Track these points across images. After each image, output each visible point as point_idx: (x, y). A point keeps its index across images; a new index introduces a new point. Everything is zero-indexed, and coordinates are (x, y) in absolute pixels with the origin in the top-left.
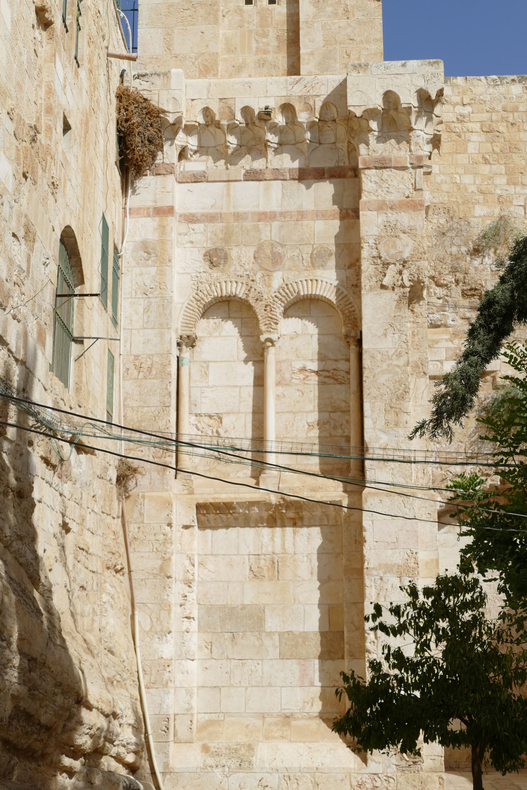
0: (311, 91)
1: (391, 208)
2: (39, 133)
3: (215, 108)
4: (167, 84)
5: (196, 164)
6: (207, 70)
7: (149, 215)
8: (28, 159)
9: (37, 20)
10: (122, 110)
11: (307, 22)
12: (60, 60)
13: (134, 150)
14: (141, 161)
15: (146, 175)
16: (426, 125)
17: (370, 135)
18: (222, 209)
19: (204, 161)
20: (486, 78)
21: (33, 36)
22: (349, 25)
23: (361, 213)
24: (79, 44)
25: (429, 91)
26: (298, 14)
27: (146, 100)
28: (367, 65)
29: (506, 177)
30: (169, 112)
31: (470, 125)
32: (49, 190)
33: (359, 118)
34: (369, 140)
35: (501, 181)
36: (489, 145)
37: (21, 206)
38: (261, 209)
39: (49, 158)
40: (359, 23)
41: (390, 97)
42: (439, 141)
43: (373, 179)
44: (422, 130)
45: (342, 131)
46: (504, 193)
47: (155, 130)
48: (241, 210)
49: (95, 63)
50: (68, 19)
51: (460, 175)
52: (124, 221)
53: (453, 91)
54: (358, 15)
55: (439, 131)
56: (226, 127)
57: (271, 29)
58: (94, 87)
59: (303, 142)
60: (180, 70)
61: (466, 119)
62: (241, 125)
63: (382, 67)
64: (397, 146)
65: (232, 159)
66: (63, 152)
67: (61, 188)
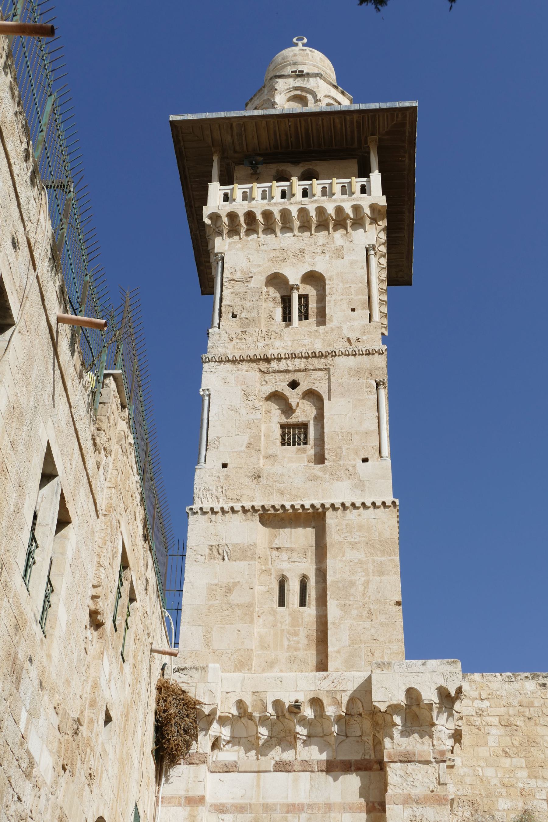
0: (338, 687)
1: (417, 803)
2: (81, 725)
3: (248, 700)
4: (205, 677)
5: (229, 754)
6: (242, 664)
7: (180, 805)
8: (69, 752)
9: (90, 621)
10: (161, 701)
11: (334, 623)
12: (108, 657)
13: (170, 739)
14: (176, 750)
15: (180, 764)
16: (447, 720)
17: (394, 730)
18: (252, 799)
19: (235, 751)
20: (501, 675)
21: (85, 636)
22: (373, 627)
23: (387, 806)
24: (126, 642)
25: (449, 689)
26: (326, 616)
27: (184, 692)
28: (390, 664)
29: (527, 770)
30: (205, 704)
31: (489, 719)
32: (86, 781)
33: (383, 712)
34: (393, 734)
35: (523, 774)
36: (508, 738)
37: (57, 798)
38: (290, 801)
39: (88, 750)
40: (381, 624)
41: (412, 694)
42: (460, 735)
43: (398, 773)
44: (443, 725)
45: (367, 724)
46: (527, 787)
47: (191, 720)
48: (270, 801)
49: (139, 658)
50: (118, 620)
51: (482, 768)
52: (155, 810)
53: (471, 686)
54: (381, 618)
55: (460, 726)
56: (257, 719)
57: (301, 629)
58: (137, 680)
59: (330, 734)
60: (217, 665)
61: (485, 713)
62: (271, 717)
63: (404, 666)
64: (420, 741)
65: (263, 750)
66: (102, 743)
67: (97, 779)
